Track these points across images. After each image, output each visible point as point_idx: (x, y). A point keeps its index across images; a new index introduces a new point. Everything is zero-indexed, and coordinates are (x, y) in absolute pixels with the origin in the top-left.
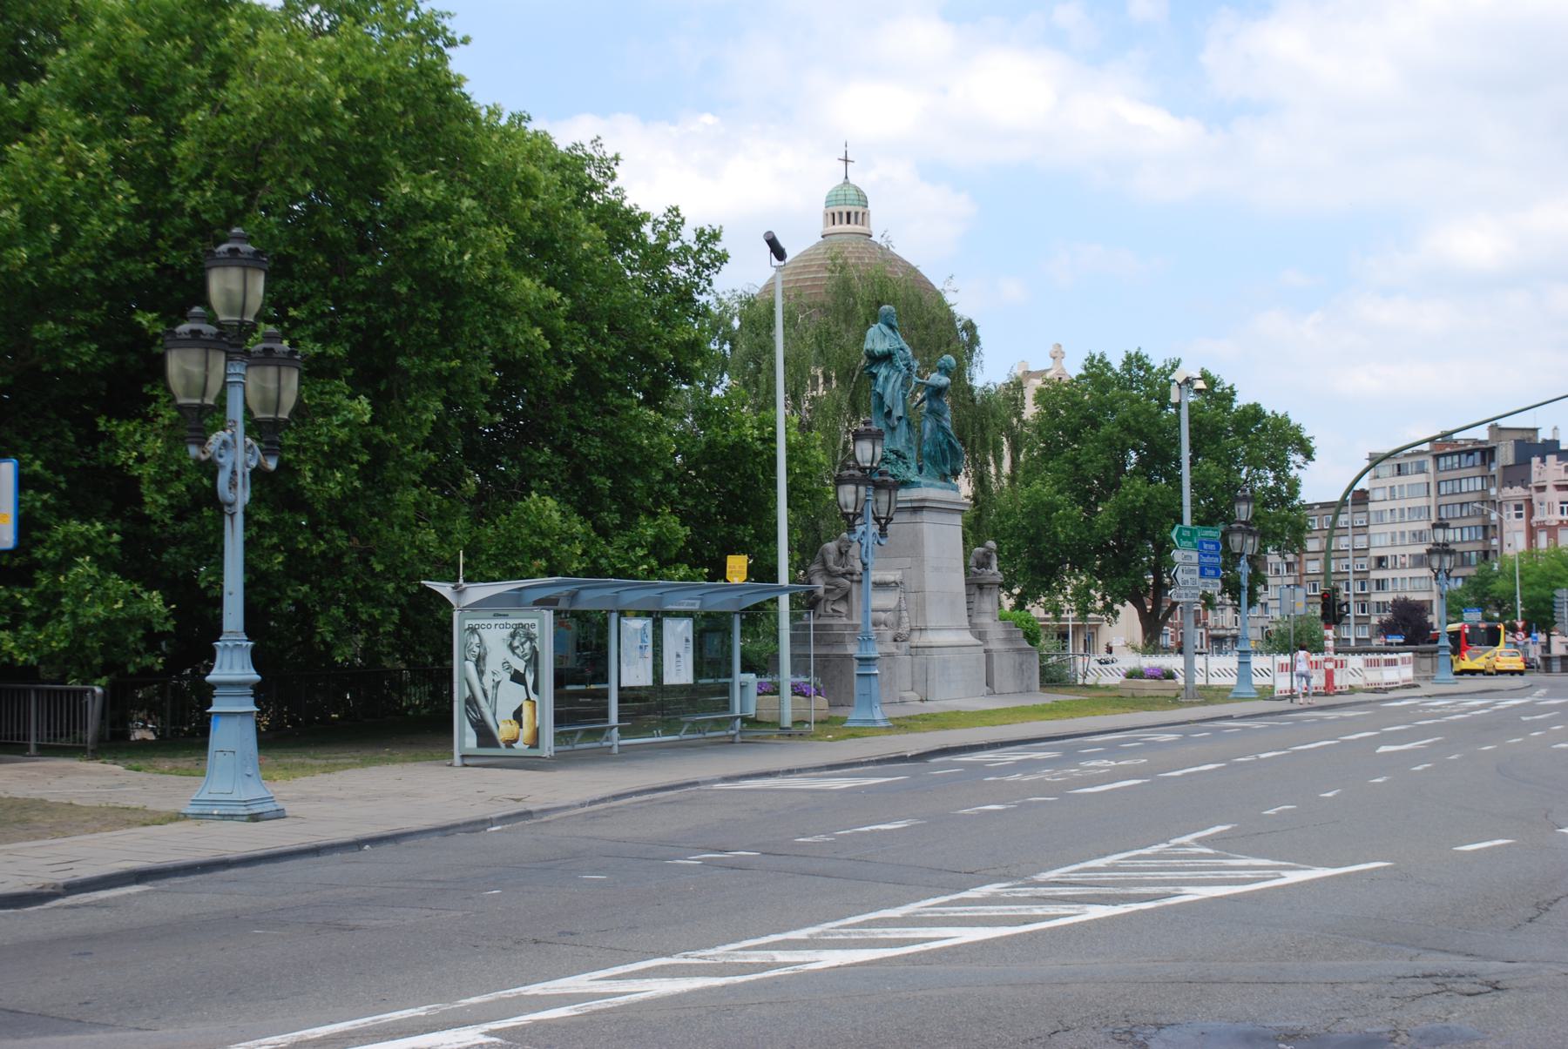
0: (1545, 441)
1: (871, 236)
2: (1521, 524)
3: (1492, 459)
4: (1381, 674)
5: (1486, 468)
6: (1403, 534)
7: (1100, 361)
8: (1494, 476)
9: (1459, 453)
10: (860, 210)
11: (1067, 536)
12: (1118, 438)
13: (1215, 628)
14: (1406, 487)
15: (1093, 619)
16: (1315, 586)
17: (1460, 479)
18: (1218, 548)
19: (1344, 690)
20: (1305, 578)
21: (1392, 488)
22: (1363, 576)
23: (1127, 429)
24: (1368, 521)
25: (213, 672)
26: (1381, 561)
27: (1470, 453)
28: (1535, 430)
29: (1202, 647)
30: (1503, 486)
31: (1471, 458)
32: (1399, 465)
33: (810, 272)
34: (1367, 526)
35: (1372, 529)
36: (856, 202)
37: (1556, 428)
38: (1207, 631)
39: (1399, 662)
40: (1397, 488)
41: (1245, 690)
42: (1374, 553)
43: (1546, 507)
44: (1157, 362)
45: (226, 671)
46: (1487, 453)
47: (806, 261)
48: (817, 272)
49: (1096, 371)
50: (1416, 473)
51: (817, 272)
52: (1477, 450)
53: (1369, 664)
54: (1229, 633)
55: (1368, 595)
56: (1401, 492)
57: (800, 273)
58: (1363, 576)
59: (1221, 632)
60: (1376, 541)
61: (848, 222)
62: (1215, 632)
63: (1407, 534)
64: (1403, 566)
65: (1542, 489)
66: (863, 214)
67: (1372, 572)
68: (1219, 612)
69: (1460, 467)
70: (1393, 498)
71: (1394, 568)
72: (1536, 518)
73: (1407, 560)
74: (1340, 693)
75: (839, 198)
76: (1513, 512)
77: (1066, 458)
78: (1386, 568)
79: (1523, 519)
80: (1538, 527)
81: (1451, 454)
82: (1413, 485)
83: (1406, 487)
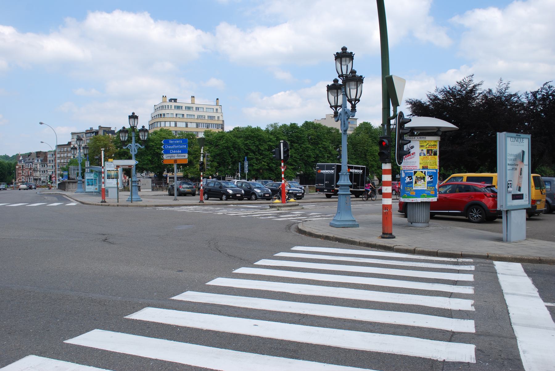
13: (35, 177)
25: (338, 182)
28: (110, 128)
29: (32, 181)
32: (78, 136)
37: (116, 128)
38: (33, 177)
45: (342, 181)
54: (38, 178)
59: (36, 178)
62: (35, 178)
68: (36, 172)
69: (91, 136)
82: (188, 115)
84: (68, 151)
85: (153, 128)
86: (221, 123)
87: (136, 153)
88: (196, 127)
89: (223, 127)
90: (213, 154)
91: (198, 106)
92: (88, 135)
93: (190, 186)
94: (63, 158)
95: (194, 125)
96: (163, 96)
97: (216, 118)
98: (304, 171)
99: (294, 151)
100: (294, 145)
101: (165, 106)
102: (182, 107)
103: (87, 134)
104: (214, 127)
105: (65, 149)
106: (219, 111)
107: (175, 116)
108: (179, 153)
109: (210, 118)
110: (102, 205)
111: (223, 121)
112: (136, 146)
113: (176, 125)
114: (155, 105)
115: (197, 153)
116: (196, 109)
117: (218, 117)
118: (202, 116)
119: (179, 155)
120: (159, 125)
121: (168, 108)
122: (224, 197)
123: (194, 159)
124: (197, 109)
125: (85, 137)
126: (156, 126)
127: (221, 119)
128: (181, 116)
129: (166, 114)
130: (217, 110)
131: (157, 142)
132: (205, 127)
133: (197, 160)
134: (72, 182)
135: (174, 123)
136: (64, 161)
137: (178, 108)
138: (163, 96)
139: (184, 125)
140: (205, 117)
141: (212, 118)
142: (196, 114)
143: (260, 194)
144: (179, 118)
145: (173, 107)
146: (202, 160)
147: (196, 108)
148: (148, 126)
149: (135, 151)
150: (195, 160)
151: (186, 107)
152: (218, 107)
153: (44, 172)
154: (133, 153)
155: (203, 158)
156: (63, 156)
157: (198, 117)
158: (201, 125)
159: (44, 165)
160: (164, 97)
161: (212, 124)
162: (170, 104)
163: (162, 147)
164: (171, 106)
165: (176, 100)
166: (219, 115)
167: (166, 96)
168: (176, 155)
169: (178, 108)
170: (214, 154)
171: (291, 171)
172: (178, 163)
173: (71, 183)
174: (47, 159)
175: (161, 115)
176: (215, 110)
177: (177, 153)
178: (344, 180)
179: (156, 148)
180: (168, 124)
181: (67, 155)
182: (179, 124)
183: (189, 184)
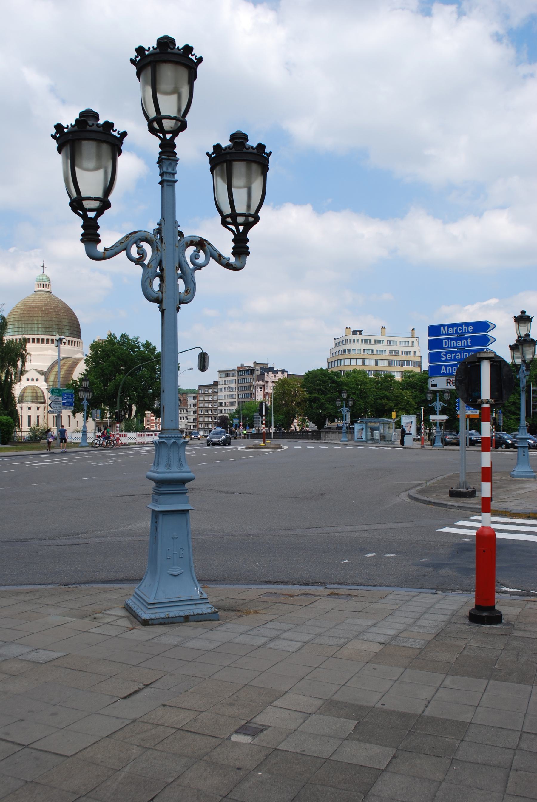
0: (270, 367)
1: (51, 292)
2: (261, 393)
3: (254, 373)
4: (145, 439)
5: (252, 375)
6: (228, 395)
7: (113, 336)
8: (254, 378)
9: (244, 370)
10: (48, 283)
11: (97, 393)
12: (116, 362)
14: (229, 381)
15: (105, 421)
16: (202, 411)
17: (244, 379)
18: (72, 395)
19: (126, 444)
20: (199, 409)
21: (225, 381)
22: (216, 408)
23: (119, 359)
24: (218, 391)
26: (221, 404)
27: (247, 370)
28: (267, 364)
30: (257, 381)
31: (248, 372)
32: (227, 374)
33: (29, 303)
34: (217, 393)
35: (219, 394)
36: (46, 281)
39: (154, 435)
40: (226, 381)
41: (84, 444)
42: (219, 401)
43: (268, 388)
44: (131, 337)
46: (252, 371)
47: (28, 299)
48: (31, 303)
49: (111, 339)
50: (232, 376)
51: (31, 303)
52: (249, 370)
53: (138, 435)
55: (217, 414)
56: (228, 382)
57: (26, 304)
58: (216, 408)
60: (220, 398)
61: (43, 287)
63: (229, 395)
64: (228, 405)
65: (267, 382)
66: (49, 285)
67: (218, 407)
69: (244, 375)
70: (225, 384)
71: (225, 406)
72: (266, 391)
73: (229, 404)
74: (124, 445)
75: (40, 279)
76: (259, 389)
77: (99, 367)
78: (222, 406)
79: (262, 391)
80: (266, 394)
81: (242, 371)
83: (229, 381)
84: (214, 393)
85: (334, 367)
86: (419, 359)
87: (440, 410)
88: (387, 365)
89: (421, 364)
90: (417, 400)
91: (390, 339)
92: (241, 374)
93: (455, 437)
94: (207, 402)
95: (386, 363)
96: (347, 327)
97: (412, 354)
98: (531, 422)
99: (517, 396)
100: (517, 389)
101: (351, 340)
102: (370, 340)
103: (239, 372)
104: (409, 365)
105: (211, 390)
106: (416, 344)
107: (362, 352)
108: (472, 410)
109: (405, 353)
110: (421, 449)
111: (421, 357)
112: (440, 404)
113: (363, 363)
114: (335, 338)
115: (399, 399)
116: (388, 343)
117: (415, 352)
118: (395, 352)
119: (472, 411)
120: (342, 364)
121: (354, 342)
122: (504, 446)
123: (395, 406)
124: (389, 342)
125: (236, 376)
126: (339, 365)
127: (418, 354)
128: (370, 352)
129: (351, 350)
130: (413, 343)
131: (352, 386)
132: (399, 365)
133: (398, 407)
134: (332, 432)
135: (361, 361)
136: (208, 405)
137: (366, 341)
138: (347, 327)
139: (373, 363)
140: (398, 353)
141: (407, 354)
142: (388, 348)
143: (533, 445)
144: (367, 354)
145: (360, 341)
146: (494, 416)
147: (388, 341)
148: (327, 363)
149: (439, 408)
150: (396, 407)
151: (375, 341)
152: (414, 340)
153: (183, 419)
154: (438, 410)
155: (495, 414)
156: (207, 399)
157: (390, 353)
158: (399, 362)
159: (183, 410)
160: (348, 328)
161: (407, 361)
162: (355, 337)
163: (457, 404)
164: (358, 340)
165: (362, 331)
166: (415, 349)
167: (350, 328)
168: (469, 411)
169: (366, 341)
170: (419, 400)
171: (514, 421)
172: (471, 417)
173: (331, 433)
174: (187, 402)
175: (345, 350)
176: (410, 344)
177: (470, 410)
178: (169, 465)
179: (351, 393)
180: (353, 362)
181: (213, 397)
182: (367, 362)
183: (454, 435)
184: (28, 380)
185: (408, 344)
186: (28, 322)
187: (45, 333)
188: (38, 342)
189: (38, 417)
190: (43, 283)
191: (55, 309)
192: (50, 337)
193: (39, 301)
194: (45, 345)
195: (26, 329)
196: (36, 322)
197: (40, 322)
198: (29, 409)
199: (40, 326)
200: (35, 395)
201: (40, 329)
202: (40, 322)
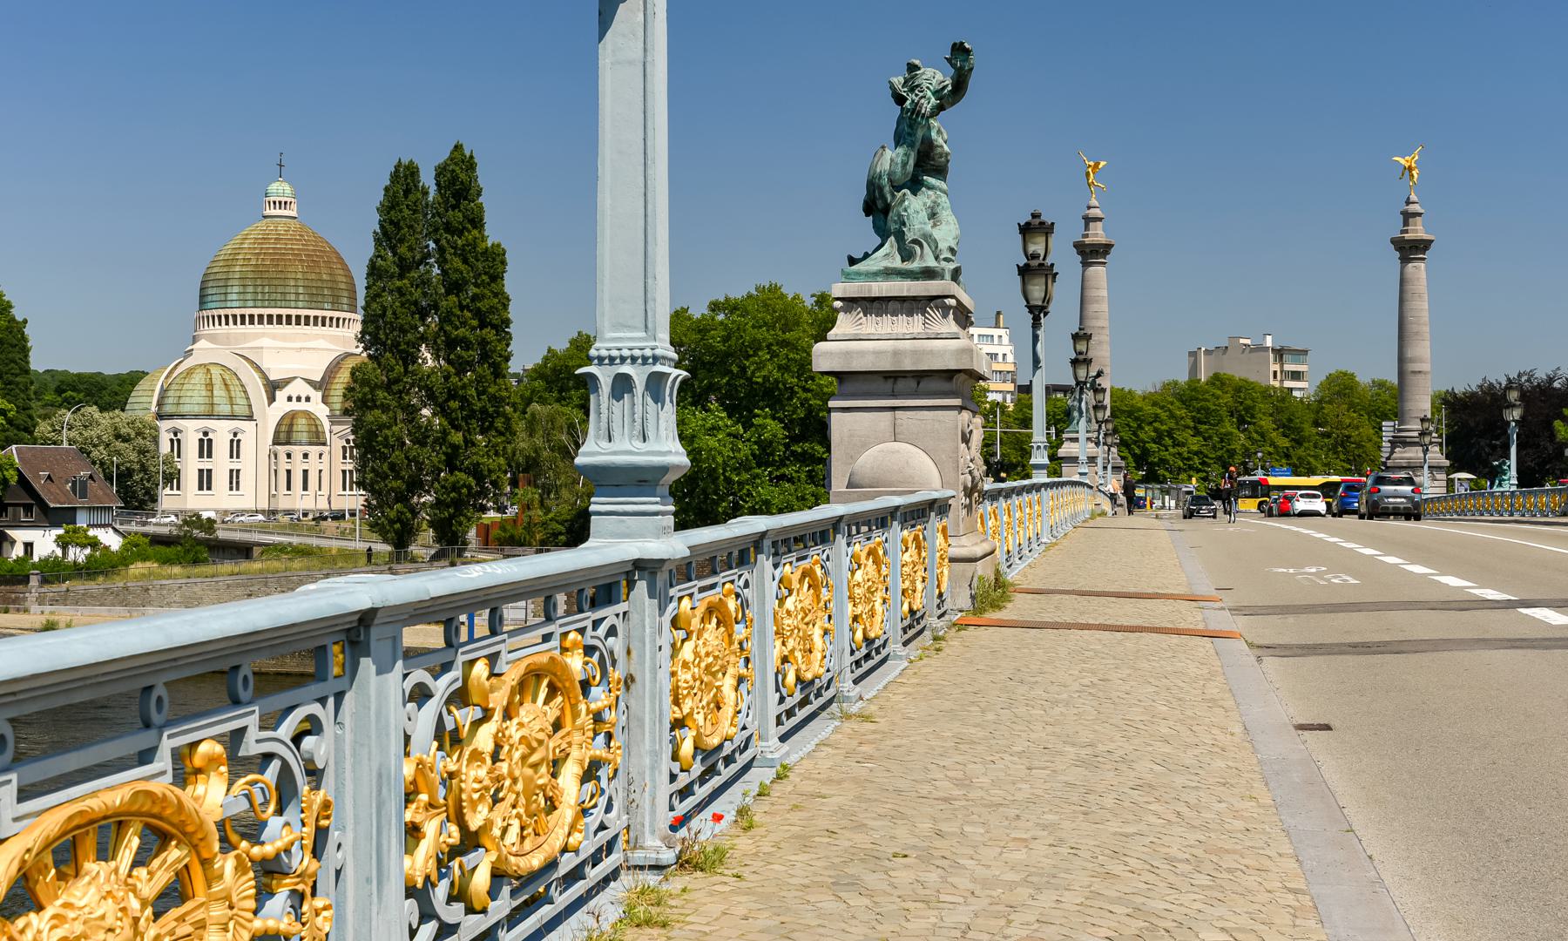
57: (262, 243)
97: (1000, 358)
117: (1004, 355)
184: (290, 399)
185: (993, 340)
186: (276, 282)
187: (314, 300)
188: (316, 324)
189: (320, 471)
190: (286, 199)
191: (322, 257)
192: (319, 313)
193: (289, 239)
194: (311, 329)
195: (273, 296)
196: (292, 283)
197: (301, 283)
198: (306, 456)
199: (301, 290)
200: (314, 429)
201: (301, 297)
202: (301, 283)
